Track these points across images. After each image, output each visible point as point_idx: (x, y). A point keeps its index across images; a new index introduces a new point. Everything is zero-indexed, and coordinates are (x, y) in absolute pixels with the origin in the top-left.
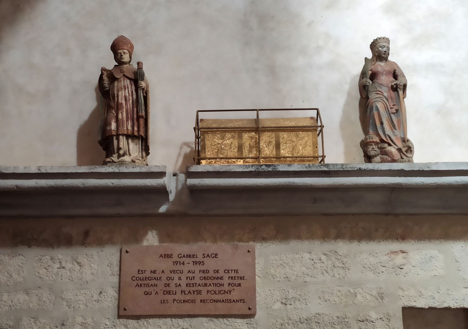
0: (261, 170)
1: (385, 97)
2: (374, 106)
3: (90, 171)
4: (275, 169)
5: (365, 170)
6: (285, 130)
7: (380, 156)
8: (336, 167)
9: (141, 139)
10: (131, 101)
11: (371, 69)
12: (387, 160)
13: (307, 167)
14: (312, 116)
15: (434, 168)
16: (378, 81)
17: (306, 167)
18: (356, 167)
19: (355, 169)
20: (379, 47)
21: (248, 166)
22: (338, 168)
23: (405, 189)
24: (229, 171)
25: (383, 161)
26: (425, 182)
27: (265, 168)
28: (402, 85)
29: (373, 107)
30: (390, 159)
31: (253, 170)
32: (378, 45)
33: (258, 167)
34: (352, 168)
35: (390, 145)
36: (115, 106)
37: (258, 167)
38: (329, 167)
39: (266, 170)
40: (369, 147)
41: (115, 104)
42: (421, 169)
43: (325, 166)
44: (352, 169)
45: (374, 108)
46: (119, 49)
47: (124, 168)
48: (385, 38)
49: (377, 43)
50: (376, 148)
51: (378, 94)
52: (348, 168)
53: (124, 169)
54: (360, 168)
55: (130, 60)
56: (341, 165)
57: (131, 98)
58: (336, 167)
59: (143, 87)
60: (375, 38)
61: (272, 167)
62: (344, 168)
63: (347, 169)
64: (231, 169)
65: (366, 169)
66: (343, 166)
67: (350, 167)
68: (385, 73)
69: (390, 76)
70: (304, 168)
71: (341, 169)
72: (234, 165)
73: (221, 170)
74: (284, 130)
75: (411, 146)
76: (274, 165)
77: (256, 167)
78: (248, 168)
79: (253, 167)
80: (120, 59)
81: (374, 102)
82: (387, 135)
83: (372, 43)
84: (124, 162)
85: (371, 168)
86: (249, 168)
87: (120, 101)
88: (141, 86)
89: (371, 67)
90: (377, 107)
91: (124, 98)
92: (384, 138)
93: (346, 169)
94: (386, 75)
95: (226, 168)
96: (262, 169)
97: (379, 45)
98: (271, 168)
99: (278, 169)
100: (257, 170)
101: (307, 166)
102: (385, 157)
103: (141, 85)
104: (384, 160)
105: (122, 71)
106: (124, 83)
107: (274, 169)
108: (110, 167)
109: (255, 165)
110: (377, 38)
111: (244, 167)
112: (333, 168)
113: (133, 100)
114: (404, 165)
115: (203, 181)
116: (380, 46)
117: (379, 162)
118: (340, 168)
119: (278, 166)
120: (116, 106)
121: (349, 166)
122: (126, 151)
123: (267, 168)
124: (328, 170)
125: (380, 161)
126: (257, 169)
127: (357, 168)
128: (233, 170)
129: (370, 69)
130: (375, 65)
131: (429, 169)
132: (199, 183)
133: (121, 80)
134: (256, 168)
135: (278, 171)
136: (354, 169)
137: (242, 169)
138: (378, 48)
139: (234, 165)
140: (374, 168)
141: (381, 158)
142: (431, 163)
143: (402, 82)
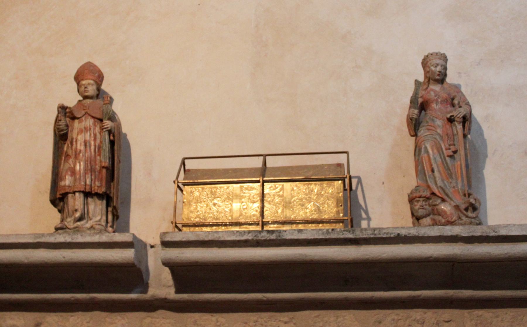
0: (260, 239)
1: (439, 134)
2: (423, 146)
3: (36, 241)
4: (279, 236)
5: (405, 236)
6: (455, 169)
7: (431, 216)
8: (364, 232)
9: (105, 198)
10: (93, 148)
11: (421, 96)
12: (439, 221)
13: (325, 234)
14: (339, 163)
15: (503, 232)
16: (431, 112)
17: (323, 234)
18: (393, 233)
19: (392, 236)
20: (430, 65)
21: (243, 232)
22: (368, 234)
23: (465, 262)
24: (217, 239)
25: (435, 223)
26: (492, 253)
27: (266, 235)
28: (461, 117)
29: (421, 148)
30: (443, 221)
31: (250, 238)
32: (429, 63)
33: (257, 235)
34: (387, 234)
35: (443, 200)
36: (72, 154)
37: (256, 234)
38: (354, 232)
39: (268, 239)
40: (416, 203)
41: (72, 152)
42: (484, 235)
43: (349, 232)
44: (388, 236)
45: (423, 150)
46: (83, 80)
47: (79, 236)
48: (438, 54)
49: (428, 60)
50: (426, 205)
51: (429, 129)
52: (381, 234)
53: (79, 239)
54: (398, 234)
55: (98, 93)
56: (372, 230)
57: (92, 143)
58: (364, 232)
59: (109, 129)
60: (426, 54)
61: (276, 233)
62: (375, 235)
63: (381, 235)
64: (220, 237)
65: (408, 235)
66: (374, 231)
67: (385, 233)
68: (439, 100)
69: (447, 105)
70: (321, 234)
71: (372, 236)
72: (224, 232)
73: (206, 239)
74: (454, 168)
75: (472, 201)
76: (279, 232)
77: (254, 234)
78: (242, 236)
79: (250, 234)
80: (83, 92)
81: (423, 141)
82: (439, 187)
83: (424, 61)
84: (80, 228)
85: (415, 233)
86: (245, 236)
87: (79, 147)
88: (106, 127)
89: (421, 93)
90: (426, 148)
91: (83, 144)
92: (436, 191)
93: (380, 236)
94: (441, 103)
95: (214, 235)
96: (262, 237)
97: (431, 63)
98: (274, 235)
99: (284, 236)
100: (255, 238)
101: (324, 233)
102: (438, 218)
103: (107, 125)
104: (436, 221)
105: (85, 108)
106: (86, 124)
107: (278, 237)
108: (61, 236)
109: (253, 232)
110: (428, 54)
111: (238, 234)
112: (361, 234)
113: (95, 145)
114: (461, 229)
115: (183, 253)
116: (432, 64)
117: (430, 226)
118: (371, 234)
119: (284, 232)
120: (74, 153)
121: (384, 231)
122: (83, 213)
123: (268, 235)
124: (353, 237)
125: (431, 223)
126: (256, 236)
127: (394, 234)
128: (222, 239)
129: (420, 95)
130: (428, 90)
131: (496, 234)
132: (177, 257)
133: (82, 119)
134: (253, 236)
135: (284, 239)
136: (390, 235)
137: (234, 236)
138: (429, 67)
139: (224, 232)
140: (418, 233)
141: (433, 220)
142: (499, 226)
143: (460, 112)
